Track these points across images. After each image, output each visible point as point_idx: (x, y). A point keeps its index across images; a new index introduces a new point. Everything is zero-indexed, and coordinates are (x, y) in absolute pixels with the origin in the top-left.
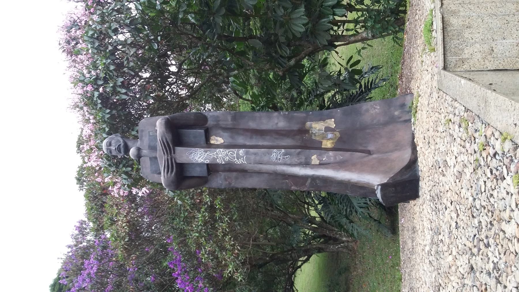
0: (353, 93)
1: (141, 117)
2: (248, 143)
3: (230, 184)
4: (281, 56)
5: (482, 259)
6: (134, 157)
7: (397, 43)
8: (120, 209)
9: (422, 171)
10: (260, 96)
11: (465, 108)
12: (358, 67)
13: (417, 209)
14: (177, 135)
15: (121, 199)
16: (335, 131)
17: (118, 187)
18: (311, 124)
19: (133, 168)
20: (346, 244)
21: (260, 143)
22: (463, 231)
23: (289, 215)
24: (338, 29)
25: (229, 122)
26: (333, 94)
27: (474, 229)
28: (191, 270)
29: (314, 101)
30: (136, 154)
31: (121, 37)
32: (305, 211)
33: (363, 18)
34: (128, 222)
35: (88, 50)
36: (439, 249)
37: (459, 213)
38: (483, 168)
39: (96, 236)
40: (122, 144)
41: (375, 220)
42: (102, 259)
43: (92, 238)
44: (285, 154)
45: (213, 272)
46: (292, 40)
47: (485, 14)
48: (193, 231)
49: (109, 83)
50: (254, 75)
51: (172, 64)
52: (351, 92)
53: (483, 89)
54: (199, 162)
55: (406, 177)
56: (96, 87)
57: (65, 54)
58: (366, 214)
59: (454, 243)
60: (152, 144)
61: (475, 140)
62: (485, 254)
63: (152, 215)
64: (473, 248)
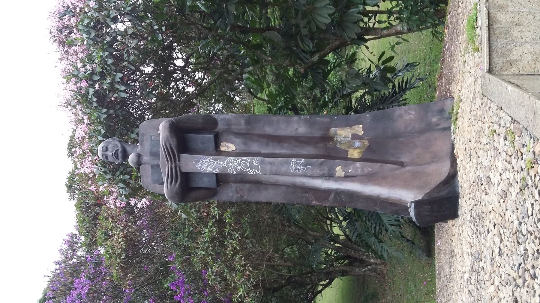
0: (384, 94)
1: (141, 118)
2: (263, 151)
3: (242, 197)
4: (303, 51)
5: (527, 292)
6: (134, 164)
7: (437, 38)
8: (116, 222)
11: (512, 119)
12: (391, 64)
13: (455, 230)
14: (183, 139)
15: (118, 211)
16: (364, 139)
17: (114, 197)
18: (336, 131)
19: (131, 176)
20: (374, 267)
21: (277, 151)
23: (309, 232)
24: (369, 20)
25: (242, 126)
26: (362, 94)
28: (196, 293)
29: (340, 102)
30: (135, 160)
31: (121, 27)
32: (328, 228)
34: (125, 237)
35: (83, 41)
36: (480, 278)
37: (503, 238)
38: (531, 188)
39: (88, 251)
41: (408, 240)
42: (94, 278)
44: (306, 164)
50: (272, 71)
51: (178, 58)
52: (382, 93)
53: (533, 98)
55: (444, 193)
56: (91, 83)
57: (56, 44)
58: (398, 233)
59: (497, 272)
60: (155, 150)
61: (522, 155)
62: (531, 286)
63: (152, 229)
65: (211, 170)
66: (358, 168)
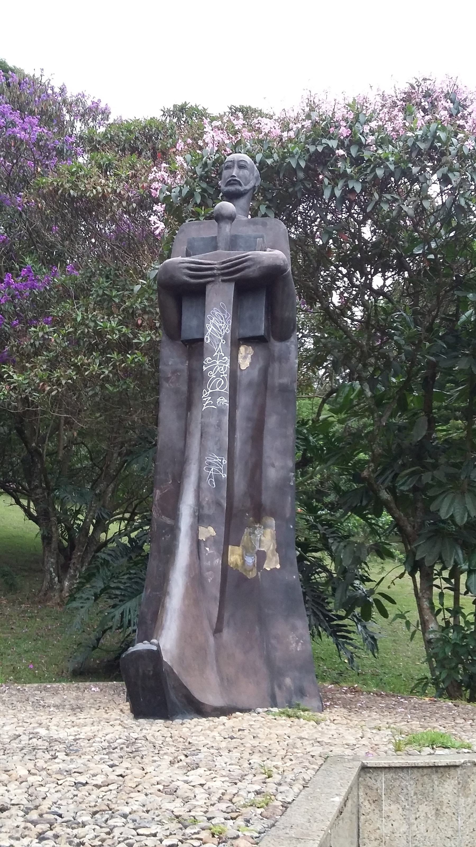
0: (328, 603)
1: (290, 221)
2: (239, 413)
3: (167, 379)
4: (396, 476)
5: (18, 827)
6: (218, 210)
8: (127, 182)
9: (182, 724)
10: (326, 436)
11: (289, 803)
12: (375, 614)
13: (115, 714)
14: (257, 288)
15: (145, 185)
17: (166, 178)
18: (270, 527)
19: (200, 206)
20: (57, 587)
21: (238, 435)
22: (70, 795)
23: (112, 485)
24: (445, 579)
25: (279, 379)
26: (328, 567)
27: (73, 815)
28: (15, 307)
30: (224, 212)
31: (434, 190)
32: (118, 514)
33: (462, 624)
35: (412, 130)
36: (40, 753)
38: (181, 832)
39: (81, 138)
40: (241, 189)
41: (98, 640)
42: (39, 147)
43: (77, 131)
44: (218, 480)
45: (12, 347)
46: (426, 495)
47: (461, 842)
48: (86, 311)
49: (352, 165)
51: (385, 280)
52: (330, 600)
53: (321, 835)
54: (207, 325)
55: (173, 695)
56: (346, 142)
57: (406, 87)
58: (110, 624)
59: (49, 779)
60: (241, 242)
61: (232, 819)
62: (27, 833)
63: (116, 239)
64: (39, 811)
65: (210, 331)
66: (212, 562)
